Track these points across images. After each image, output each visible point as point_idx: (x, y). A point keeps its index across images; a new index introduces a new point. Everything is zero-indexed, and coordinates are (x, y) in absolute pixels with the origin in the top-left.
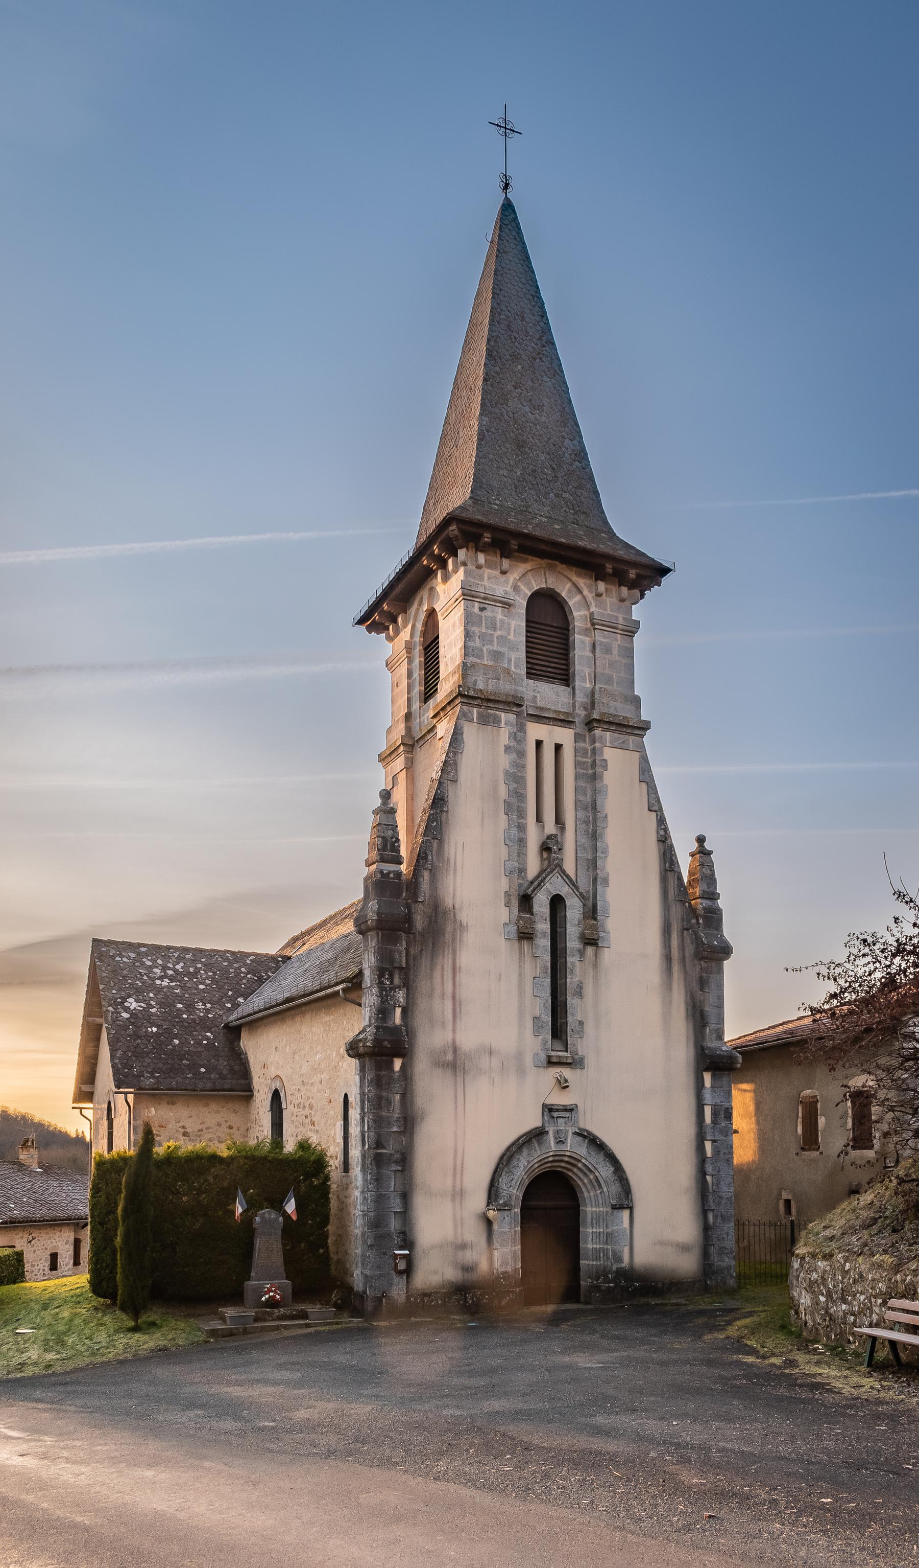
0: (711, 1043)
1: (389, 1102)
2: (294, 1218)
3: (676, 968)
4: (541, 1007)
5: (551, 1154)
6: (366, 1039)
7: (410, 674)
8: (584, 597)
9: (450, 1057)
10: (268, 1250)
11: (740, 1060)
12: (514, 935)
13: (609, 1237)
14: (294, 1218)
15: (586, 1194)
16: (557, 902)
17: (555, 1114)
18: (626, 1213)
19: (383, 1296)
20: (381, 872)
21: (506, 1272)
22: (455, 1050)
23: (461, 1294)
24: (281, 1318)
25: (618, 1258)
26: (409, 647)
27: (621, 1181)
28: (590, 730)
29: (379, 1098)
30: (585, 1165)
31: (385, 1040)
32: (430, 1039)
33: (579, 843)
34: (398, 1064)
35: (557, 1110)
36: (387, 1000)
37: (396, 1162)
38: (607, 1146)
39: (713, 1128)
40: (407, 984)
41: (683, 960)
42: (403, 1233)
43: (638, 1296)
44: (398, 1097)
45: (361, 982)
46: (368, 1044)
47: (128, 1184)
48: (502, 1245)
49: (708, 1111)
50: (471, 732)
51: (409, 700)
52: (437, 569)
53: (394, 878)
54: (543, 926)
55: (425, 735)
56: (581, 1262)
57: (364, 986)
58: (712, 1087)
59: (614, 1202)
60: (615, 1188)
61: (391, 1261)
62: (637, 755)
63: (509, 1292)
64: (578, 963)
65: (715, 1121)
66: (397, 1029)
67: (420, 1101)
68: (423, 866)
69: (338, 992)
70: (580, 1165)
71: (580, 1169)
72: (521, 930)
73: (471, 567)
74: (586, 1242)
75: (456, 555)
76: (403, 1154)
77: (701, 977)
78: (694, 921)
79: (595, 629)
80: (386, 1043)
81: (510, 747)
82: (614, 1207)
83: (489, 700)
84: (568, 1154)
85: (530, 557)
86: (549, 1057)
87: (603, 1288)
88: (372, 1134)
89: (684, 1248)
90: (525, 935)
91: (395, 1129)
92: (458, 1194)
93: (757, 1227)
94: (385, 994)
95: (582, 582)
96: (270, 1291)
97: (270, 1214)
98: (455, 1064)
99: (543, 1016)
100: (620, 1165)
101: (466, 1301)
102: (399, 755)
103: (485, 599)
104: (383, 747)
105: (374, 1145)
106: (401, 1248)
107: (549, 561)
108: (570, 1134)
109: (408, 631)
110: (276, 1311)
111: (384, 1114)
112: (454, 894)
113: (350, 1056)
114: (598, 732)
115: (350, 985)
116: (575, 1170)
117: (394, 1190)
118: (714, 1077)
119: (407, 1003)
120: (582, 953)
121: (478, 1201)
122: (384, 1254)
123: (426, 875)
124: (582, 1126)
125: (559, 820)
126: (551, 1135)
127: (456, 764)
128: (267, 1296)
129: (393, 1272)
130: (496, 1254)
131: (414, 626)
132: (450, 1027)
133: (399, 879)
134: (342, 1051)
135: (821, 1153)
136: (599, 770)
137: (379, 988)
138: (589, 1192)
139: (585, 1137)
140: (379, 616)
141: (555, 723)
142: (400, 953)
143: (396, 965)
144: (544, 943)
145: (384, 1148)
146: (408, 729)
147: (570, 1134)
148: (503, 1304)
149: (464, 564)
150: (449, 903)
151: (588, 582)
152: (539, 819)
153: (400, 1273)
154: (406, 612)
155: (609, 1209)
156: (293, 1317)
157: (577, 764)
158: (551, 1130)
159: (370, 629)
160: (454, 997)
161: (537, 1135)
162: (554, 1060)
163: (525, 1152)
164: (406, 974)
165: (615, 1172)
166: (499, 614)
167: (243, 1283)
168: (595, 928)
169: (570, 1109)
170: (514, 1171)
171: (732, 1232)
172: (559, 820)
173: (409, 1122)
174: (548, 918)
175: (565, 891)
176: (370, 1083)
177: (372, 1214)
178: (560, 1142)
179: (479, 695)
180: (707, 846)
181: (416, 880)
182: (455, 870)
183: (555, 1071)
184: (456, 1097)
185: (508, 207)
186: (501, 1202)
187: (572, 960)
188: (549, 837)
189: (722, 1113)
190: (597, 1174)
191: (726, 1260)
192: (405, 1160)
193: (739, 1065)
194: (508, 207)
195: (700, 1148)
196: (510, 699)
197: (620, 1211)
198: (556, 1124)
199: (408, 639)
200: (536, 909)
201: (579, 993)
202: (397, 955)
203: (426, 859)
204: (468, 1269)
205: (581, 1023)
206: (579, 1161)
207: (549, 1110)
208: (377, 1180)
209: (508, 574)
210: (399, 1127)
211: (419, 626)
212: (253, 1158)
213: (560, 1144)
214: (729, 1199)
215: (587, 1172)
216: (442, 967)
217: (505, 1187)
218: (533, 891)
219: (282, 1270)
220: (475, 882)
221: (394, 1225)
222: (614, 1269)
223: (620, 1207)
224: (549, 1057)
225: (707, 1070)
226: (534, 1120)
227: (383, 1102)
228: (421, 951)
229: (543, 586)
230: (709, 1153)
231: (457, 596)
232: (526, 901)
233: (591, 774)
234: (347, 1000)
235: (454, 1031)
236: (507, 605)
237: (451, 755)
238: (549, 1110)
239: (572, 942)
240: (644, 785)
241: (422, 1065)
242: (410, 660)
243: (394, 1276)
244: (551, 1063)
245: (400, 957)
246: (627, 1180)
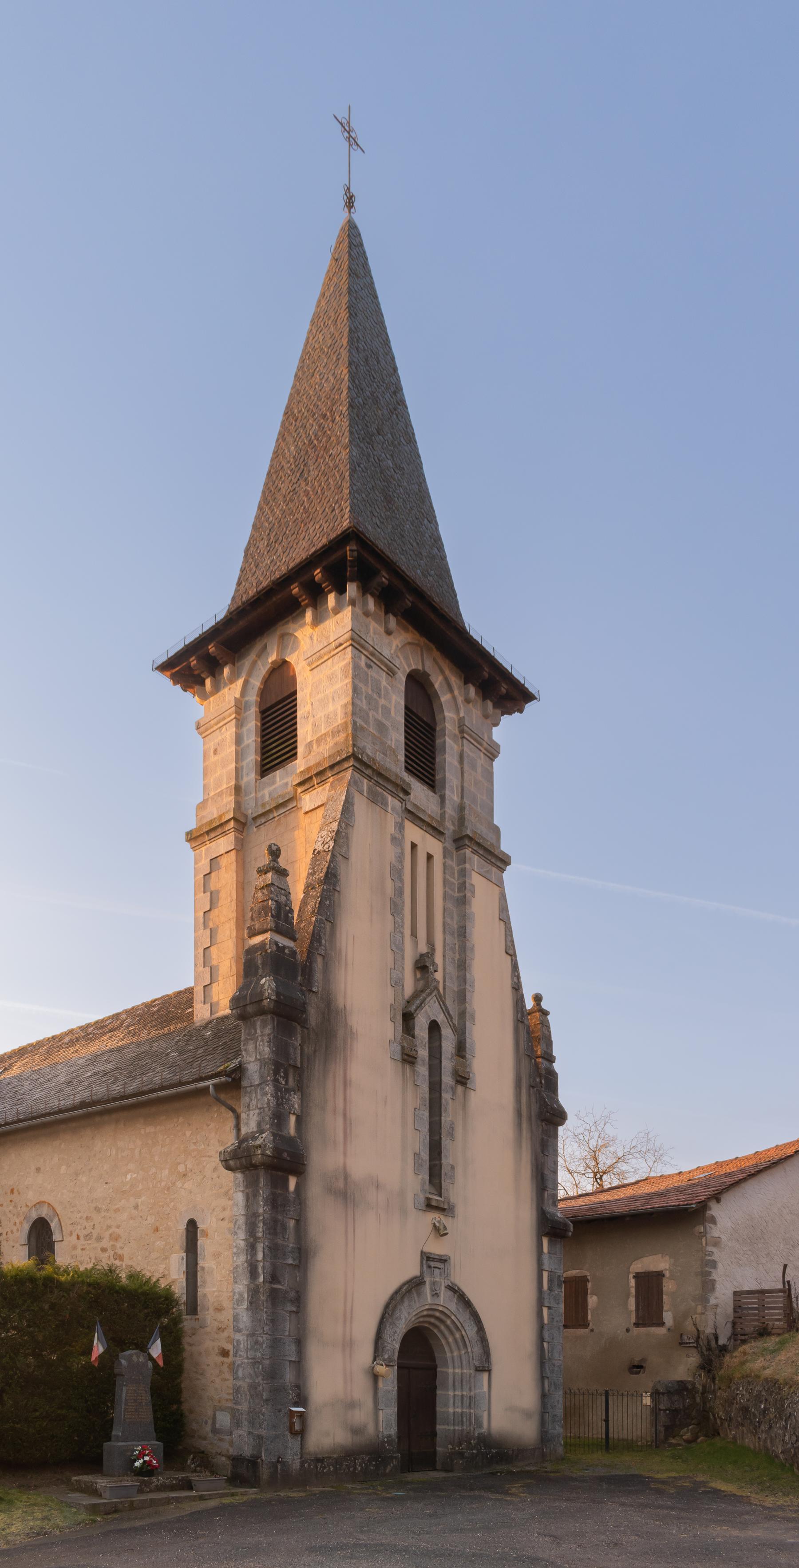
0: (550, 1209)
1: (284, 1228)
2: (161, 1363)
3: (525, 1125)
4: (419, 1142)
5: (427, 1307)
6: (265, 1146)
7: (238, 740)
8: (454, 698)
9: (341, 1184)
10: (132, 1402)
11: (572, 1229)
12: (398, 1057)
13: (472, 1401)
14: (161, 1363)
15: (448, 1354)
16: (434, 1027)
17: (432, 1264)
18: (485, 1376)
19: (278, 1461)
20: (276, 944)
22: (346, 1177)
23: (351, 1460)
24: (159, 1489)
25: (479, 1424)
26: (240, 707)
28: (458, 849)
29: (275, 1221)
31: (286, 1151)
32: (323, 1160)
33: (447, 971)
34: (292, 1182)
35: (434, 1260)
36: (282, 1103)
37: (291, 1301)
39: (549, 1294)
40: (300, 1088)
41: (530, 1118)
42: (297, 1386)
43: (492, 1465)
44: (292, 1223)
45: (240, 1079)
46: (268, 1152)
47: (259, 1276)
49: (545, 1275)
50: (361, 805)
51: (238, 771)
52: (307, 606)
53: (289, 955)
54: (423, 1053)
55: (270, 811)
56: (438, 1427)
57: (245, 1083)
58: (549, 1253)
59: (477, 1364)
60: (477, 1350)
61: (286, 1420)
62: (497, 889)
64: (450, 1101)
65: (550, 1289)
66: (290, 1141)
67: (314, 1231)
68: (317, 949)
69: (208, 1088)
70: (449, 1322)
71: (447, 1327)
72: (407, 1051)
73: (358, 610)
74: (446, 1405)
75: (341, 591)
76: (297, 1292)
77: (542, 1139)
78: (538, 1080)
79: (463, 737)
80: (285, 1155)
81: (396, 838)
83: (380, 775)
84: (441, 1308)
85: (411, 628)
86: (428, 1199)
87: (466, 1455)
88: (267, 1264)
89: (527, 1415)
90: (408, 1059)
91: (290, 1261)
92: (348, 1345)
93: (581, 1397)
94: (281, 1095)
95: (454, 681)
96: (141, 1455)
97: (138, 1357)
98: (345, 1193)
99: (422, 1153)
101: (355, 1469)
102: (224, 833)
103: (372, 654)
104: (192, 825)
105: (269, 1279)
106: (296, 1404)
107: (427, 641)
109: (236, 690)
110: (154, 1479)
111: (280, 1241)
112: (345, 993)
113: (228, 1168)
114: (468, 852)
115: (230, 1080)
116: (442, 1327)
117: (289, 1336)
118: (550, 1242)
119: (302, 1111)
120: (454, 1092)
121: (364, 1353)
122: (280, 1411)
123: (319, 960)
125: (430, 942)
126: (427, 1283)
127: (347, 838)
128: (141, 1461)
129: (287, 1433)
131: (246, 683)
132: (341, 1148)
133: (294, 958)
134: (216, 1161)
135: (592, 1330)
136: (468, 894)
137: (275, 1086)
138: (452, 1352)
140: (195, 665)
141: (428, 829)
142: (295, 1049)
143: (292, 1062)
144: (423, 1070)
145: (279, 1282)
146: (238, 805)
148: (387, 1471)
149: (353, 603)
150: (340, 1002)
151: (458, 681)
152: (414, 934)
153: (294, 1433)
154: (234, 664)
156: (173, 1488)
157: (445, 882)
158: (427, 1279)
159: (177, 679)
160: (345, 1115)
161: (414, 1285)
162: (434, 1203)
163: (406, 1303)
164: (300, 1076)
166: (384, 680)
167: (100, 1446)
168: (465, 1066)
169: (444, 1260)
171: (561, 1400)
172: (430, 942)
173: (303, 1256)
174: (427, 1045)
175: (441, 1018)
176: (266, 1201)
177: (267, 1362)
178: (436, 1295)
179: (371, 764)
180: (544, 1005)
181: (311, 963)
182: (346, 964)
183: (433, 1216)
184: (346, 1231)
185: (352, 237)
187: (446, 1096)
188: (422, 955)
189: (556, 1280)
190: (463, 1333)
191: (557, 1428)
192: (298, 1300)
193: (570, 1234)
194: (352, 237)
195: (540, 1314)
196: (399, 782)
198: (432, 1274)
199: (238, 696)
200: (417, 1031)
201: (451, 1135)
202: (292, 1051)
203: (319, 941)
204: (356, 1431)
205: (453, 1168)
206: (449, 1317)
207: (427, 1258)
208: (273, 1321)
209: (392, 637)
210: (294, 1260)
211: (256, 683)
212: (95, 1285)
214: (559, 1367)
215: (454, 1329)
216: (334, 1077)
217: (389, 1340)
218: (416, 1010)
219: (152, 1428)
220: (364, 983)
221: (289, 1376)
223: (483, 1370)
224: (428, 1199)
225: (546, 1235)
226: (412, 1270)
227: (279, 1227)
228: (315, 1051)
229: (420, 668)
230: (546, 1321)
231: (341, 640)
232: (408, 1018)
233: (460, 898)
234: (218, 1100)
235: (345, 1154)
236: (391, 673)
237: (343, 825)
238: (427, 1258)
239: (447, 1079)
240: (502, 923)
241: (315, 1190)
242: (240, 723)
243: (289, 1438)
244: (430, 1206)
245: (295, 1053)
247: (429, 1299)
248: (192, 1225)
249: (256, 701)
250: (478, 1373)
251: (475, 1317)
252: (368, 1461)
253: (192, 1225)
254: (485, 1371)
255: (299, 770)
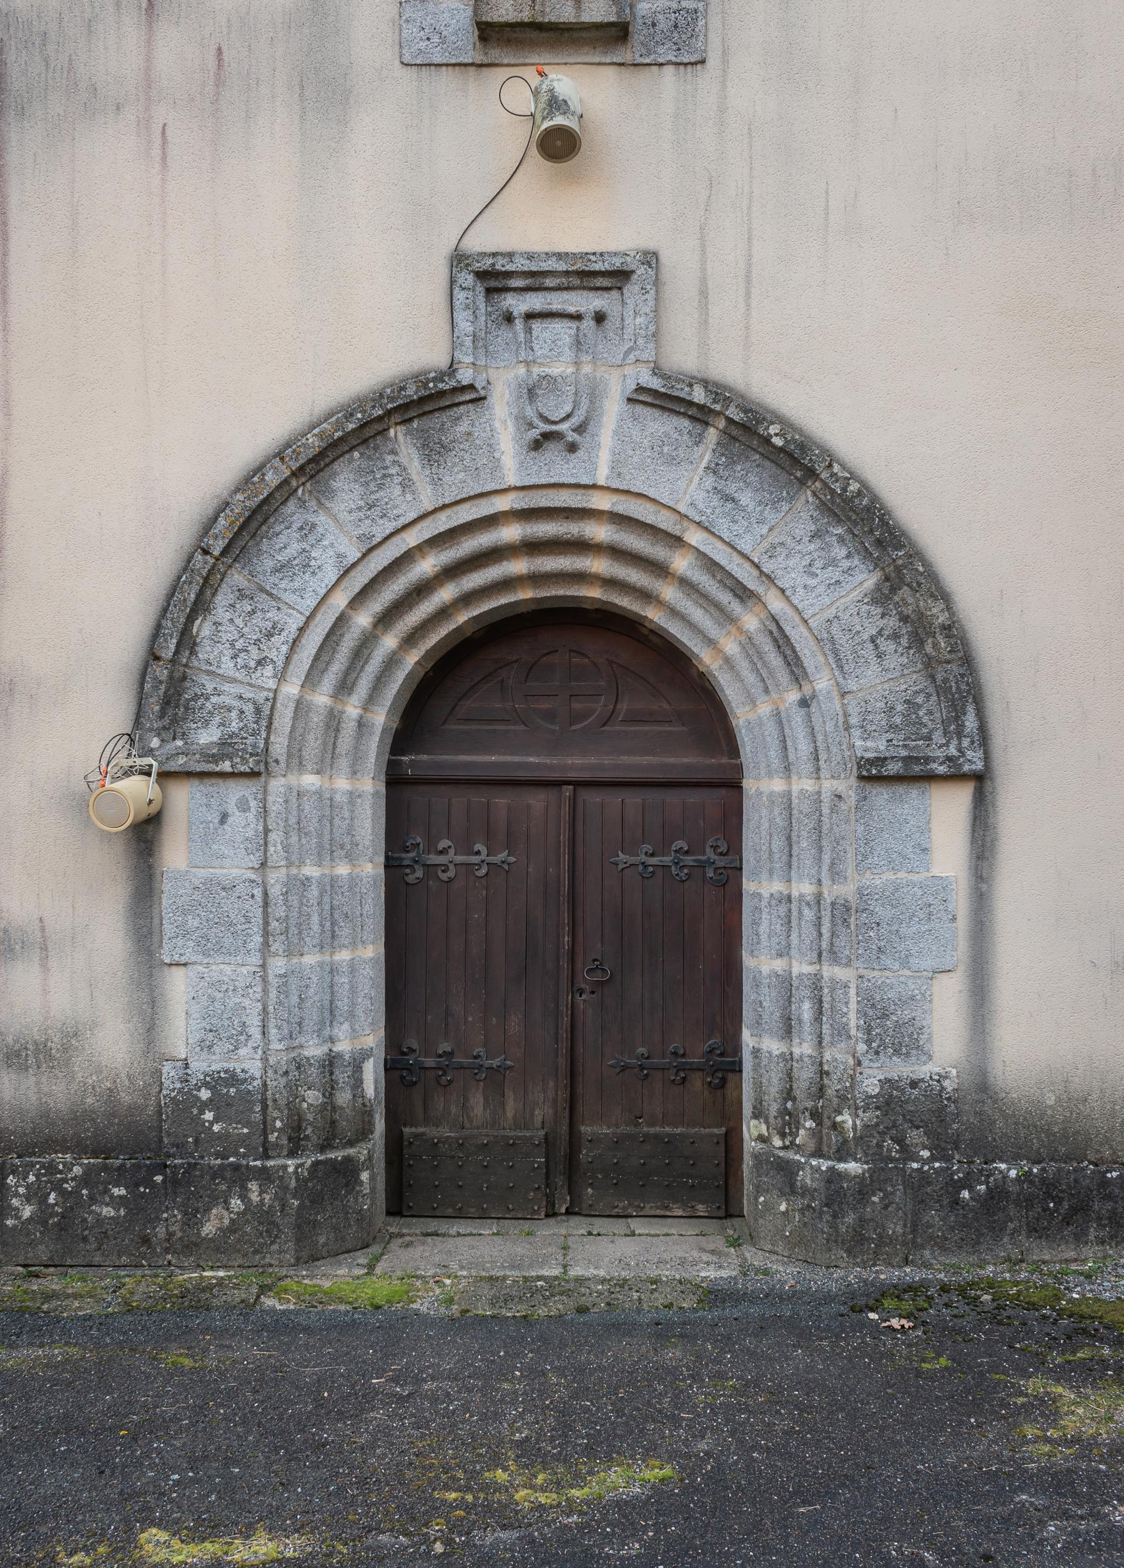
17: (519, 304)
18: (950, 807)
21: (232, 1079)
25: (891, 1028)
27: (917, 641)
30: (711, 566)
35: (536, 282)
38: (831, 458)
48: (208, 947)
59: (877, 746)
60: (883, 679)
63: (239, 1176)
82: (872, 774)
87: (805, 1178)
100: (916, 554)
108: (613, 408)
116: (669, 592)
124: (684, 355)
130: (178, 987)
139: (701, 416)
147: (613, 408)
148: (209, 1229)
155: (847, 786)
161: (428, 404)
165: (882, 597)
170: (283, 586)
183: (512, 94)
186: (207, 737)
190: (776, 604)
197: (913, 794)
213: (553, 451)
215: (724, 597)
217: (227, 667)
222: (870, 1084)
223: (916, 775)
226: (399, 333)
246: (954, 632)
247: (511, 463)
248: (219, 49)
249: (376, 794)
250: (881, 795)
251: (864, 521)
252: (85, 1180)
253: (219, 49)
254: (956, 777)
255: (371, 1060)
